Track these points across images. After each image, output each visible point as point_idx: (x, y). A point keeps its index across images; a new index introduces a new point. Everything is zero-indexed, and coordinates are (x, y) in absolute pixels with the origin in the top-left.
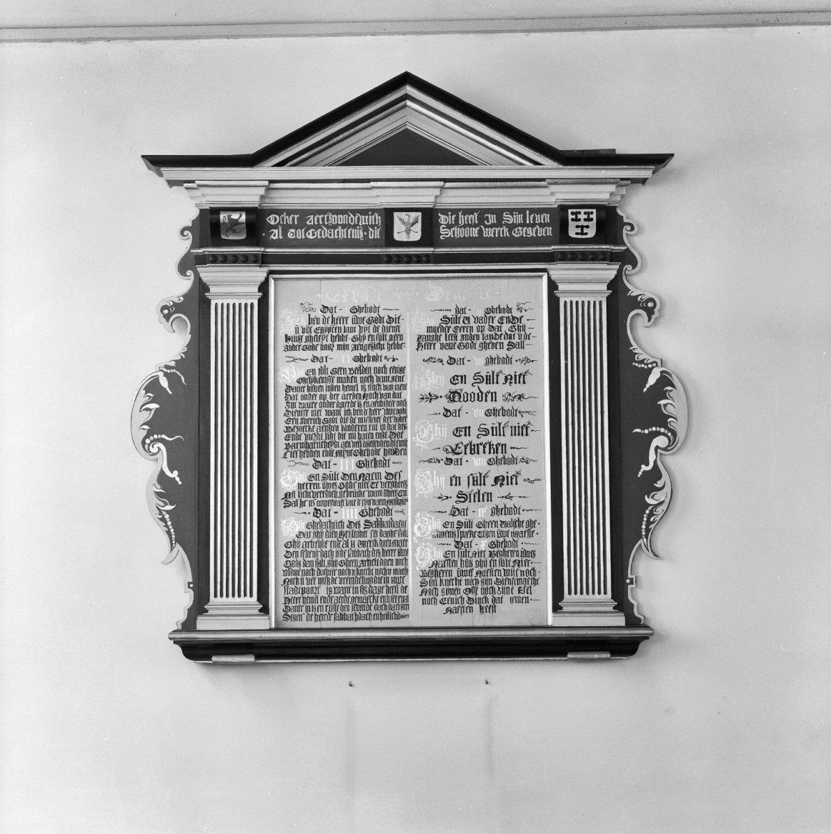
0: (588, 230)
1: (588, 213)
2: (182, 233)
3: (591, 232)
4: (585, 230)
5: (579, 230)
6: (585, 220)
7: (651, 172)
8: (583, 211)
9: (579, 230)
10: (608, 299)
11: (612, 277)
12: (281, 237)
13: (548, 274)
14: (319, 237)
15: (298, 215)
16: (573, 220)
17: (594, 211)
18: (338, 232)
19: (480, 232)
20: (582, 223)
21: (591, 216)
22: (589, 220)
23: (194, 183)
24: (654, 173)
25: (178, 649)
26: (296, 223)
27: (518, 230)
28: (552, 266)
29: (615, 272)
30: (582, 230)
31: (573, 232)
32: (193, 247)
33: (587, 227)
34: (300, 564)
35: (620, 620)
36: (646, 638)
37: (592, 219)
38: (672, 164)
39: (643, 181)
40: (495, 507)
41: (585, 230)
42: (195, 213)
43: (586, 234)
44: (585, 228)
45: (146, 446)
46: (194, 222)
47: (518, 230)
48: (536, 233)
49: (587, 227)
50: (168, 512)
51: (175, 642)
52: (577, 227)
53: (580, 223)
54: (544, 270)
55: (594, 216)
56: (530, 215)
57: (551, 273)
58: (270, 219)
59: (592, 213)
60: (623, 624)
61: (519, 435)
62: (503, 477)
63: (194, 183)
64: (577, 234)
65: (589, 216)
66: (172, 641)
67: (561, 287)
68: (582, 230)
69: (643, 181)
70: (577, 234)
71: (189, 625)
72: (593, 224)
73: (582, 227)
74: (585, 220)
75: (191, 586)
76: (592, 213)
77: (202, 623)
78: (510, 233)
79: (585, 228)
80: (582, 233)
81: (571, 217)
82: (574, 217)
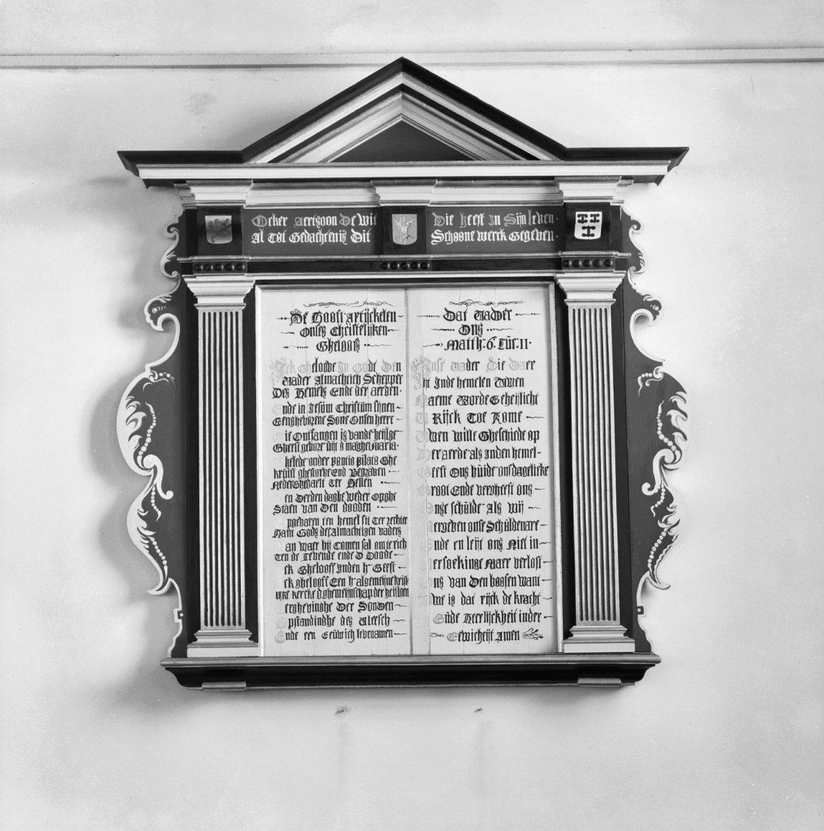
0: (576, 238)
1: (595, 216)
2: (169, 230)
3: (597, 234)
4: (592, 231)
5: (585, 232)
6: (591, 221)
7: (665, 167)
8: (589, 213)
9: (585, 232)
10: (612, 307)
11: (617, 285)
12: (262, 241)
13: (556, 284)
14: (302, 241)
15: (287, 218)
16: (579, 221)
17: (600, 213)
18: (272, 220)
19: (476, 236)
20: (589, 224)
21: (597, 218)
22: (595, 221)
23: (185, 183)
24: (669, 169)
25: (172, 678)
26: (284, 225)
27: (515, 234)
28: (558, 275)
29: (621, 280)
30: (589, 231)
31: (579, 233)
32: (177, 251)
33: (594, 228)
34: (317, 533)
35: (630, 647)
36: (652, 664)
37: (598, 221)
38: (687, 160)
39: (658, 179)
40: (475, 449)
41: (592, 231)
42: (180, 212)
43: (593, 235)
44: (586, 233)
45: (139, 458)
46: (180, 218)
47: (515, 234)
48: (535, 237)
49: (594, 228)
50: (151, 536)
51: (167, 669)
52: (584, 228)
53: (586, 225)
54: (552, 279)
55: (600, 218)
56: (532, 215)
57: (560, 281)
58: (256, 221)
59: (598, 215)
60: (633, 650)
61: (535, 475)
62: (514, 541)
63: (185, 183)
64: (584, 235)
65: (595, 218)
66: (164, 668)
67: (570, 296)
68: (589, 231)
69: (658, 179)
70: (584, 235)
71: (180, 651)
72: (599, 226)
73: (589, 228)
74: (591, 221)
75: (182, 615)
76: (598, 215)
77: (192, 652)
78: (507, 238)
79: (586, 233)
80: (589, 235)
81: (577, 219)
82: (580, 218)
